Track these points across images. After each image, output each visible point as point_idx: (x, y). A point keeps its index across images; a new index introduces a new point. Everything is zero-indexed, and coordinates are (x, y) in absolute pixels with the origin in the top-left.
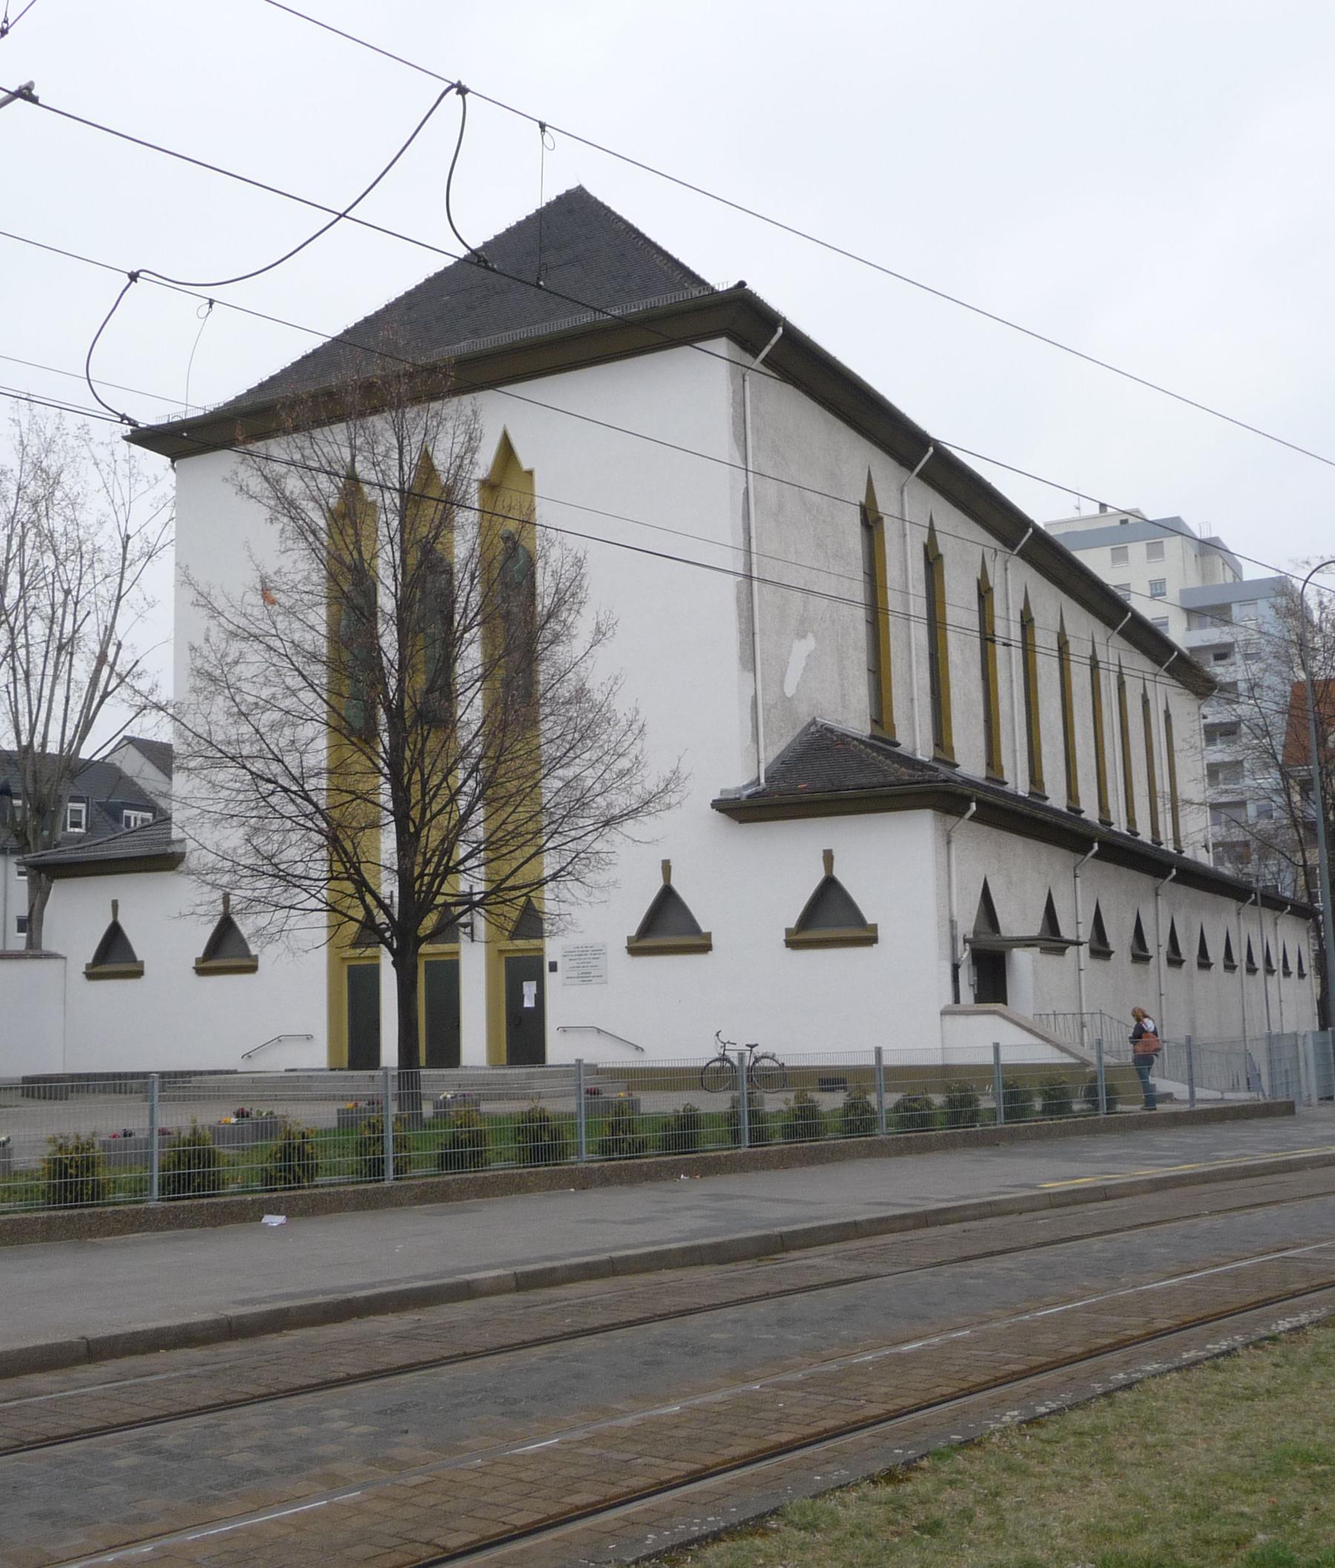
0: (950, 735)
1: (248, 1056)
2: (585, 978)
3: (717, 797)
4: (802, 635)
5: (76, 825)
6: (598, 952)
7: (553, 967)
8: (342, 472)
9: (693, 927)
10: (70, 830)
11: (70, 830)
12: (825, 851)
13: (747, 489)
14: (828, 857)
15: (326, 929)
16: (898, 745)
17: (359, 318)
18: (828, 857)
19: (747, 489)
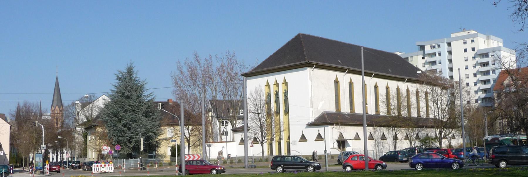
0: (354, 108)
1: (258, 154)
2: (295, 144)
3: (307, 123)
4: (322, 101)
5: (242, 113)
6: (296, 141)
7: (291, 143)
8: (81, 133)
9: (306, 139)
10: (241, 115)
11: (241, 115)
12: (492, 65)
13: (312, 85)
14: (319, 130)
15: (501, 50)
16: (341, 112)
17: (267, 58)
18: (319, 130)
19: (312, 85)
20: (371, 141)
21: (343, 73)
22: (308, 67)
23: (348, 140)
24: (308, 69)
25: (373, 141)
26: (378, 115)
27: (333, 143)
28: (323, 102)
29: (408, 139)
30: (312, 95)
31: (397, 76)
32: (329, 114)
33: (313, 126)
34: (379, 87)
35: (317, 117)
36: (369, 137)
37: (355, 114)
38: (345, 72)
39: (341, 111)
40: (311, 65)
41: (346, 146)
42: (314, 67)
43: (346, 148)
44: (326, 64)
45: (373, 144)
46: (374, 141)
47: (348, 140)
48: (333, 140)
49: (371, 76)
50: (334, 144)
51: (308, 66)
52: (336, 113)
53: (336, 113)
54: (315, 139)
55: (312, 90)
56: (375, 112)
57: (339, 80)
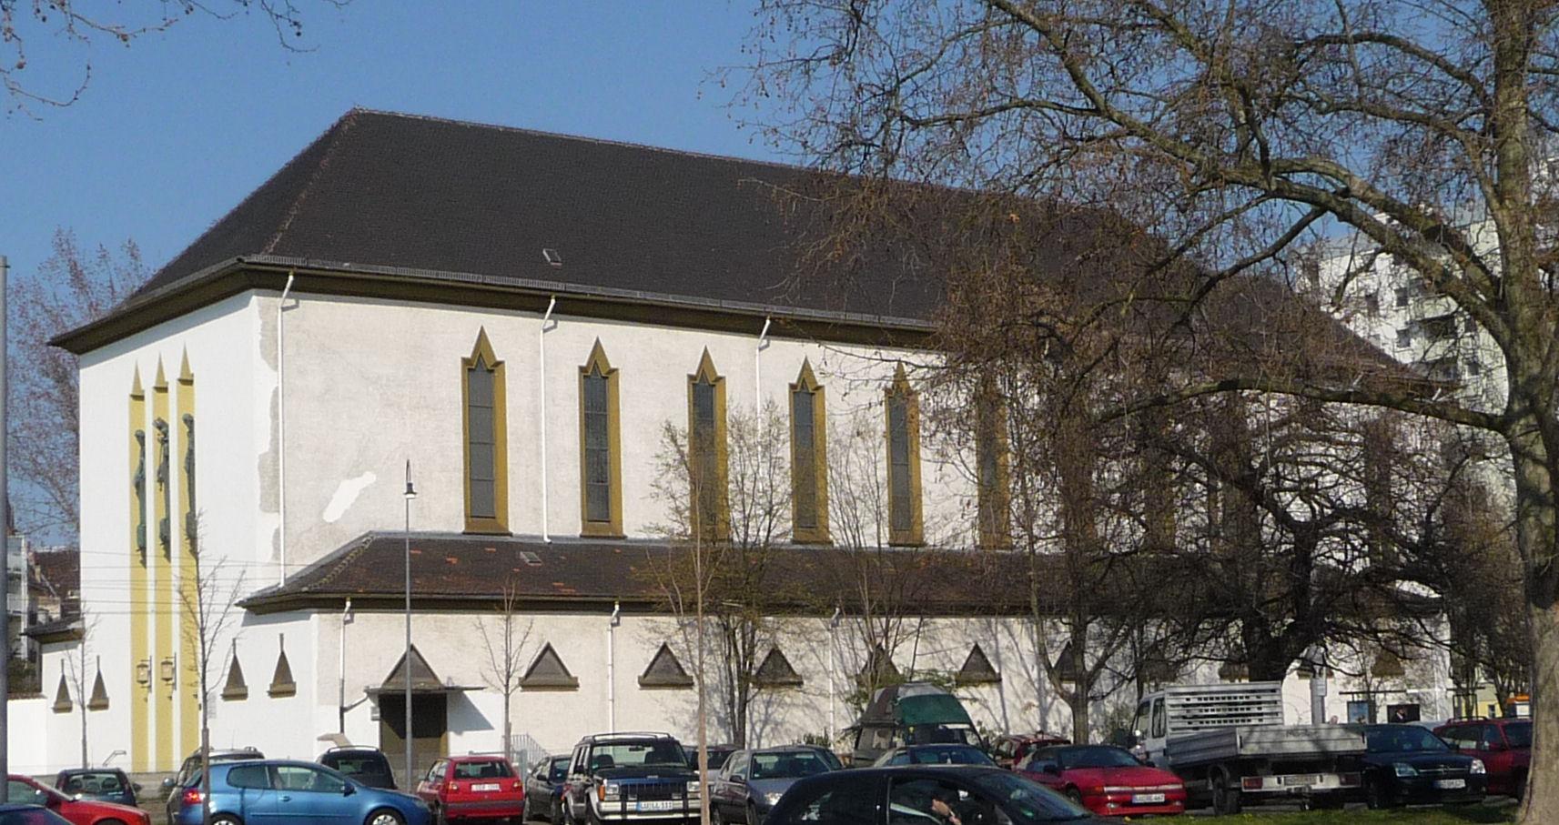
4: (354, 472)
16: (511, 535)
20: (666, 694)
21: (535, 320)
22: (253, 291)
23: (466, 692)
24: (256, 302)
25: (683, 693)
26: (817, 548)
27: (343, 710)
28: (369, 478)
29: (990, 682)
30: (275, 440)
31: (671, 299)
32: (431, 550)
33: (271, 612)
34: (826, 390)
35: (310, 561)
36: (92, 700)
37: (622, 543)
38: (546, 311)
39: (511, 530)
40: (269, 281)
41: (448, 727)
42: (553, 312)
43: (452, 735)
44: (431, 274)
45: (685, 711)
46: (693, 694)
47: (466, 692)
48: (342, 691)
49: (757, 333)
50: (346, 714)
51: (255, 287)
52: (468, 538)
53: (468, 538)
54: (272, 686)
55: (275, 416)
56: (463, 520)
57: (613, 366)
